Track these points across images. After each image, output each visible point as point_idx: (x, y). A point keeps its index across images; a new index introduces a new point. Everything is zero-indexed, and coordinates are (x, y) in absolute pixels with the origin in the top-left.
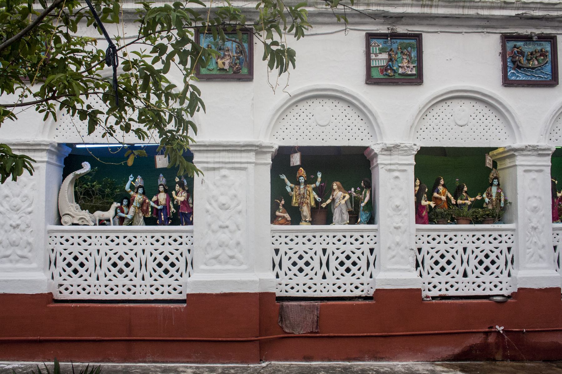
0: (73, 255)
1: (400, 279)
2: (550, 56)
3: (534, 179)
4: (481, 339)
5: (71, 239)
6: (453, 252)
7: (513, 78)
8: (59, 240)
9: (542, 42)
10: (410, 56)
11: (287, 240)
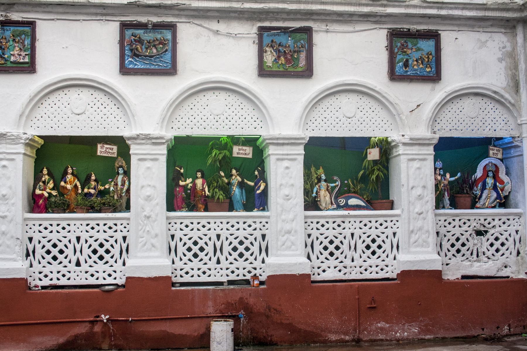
0: (98, 242)
3: (148, 168)
4: (86, 329)
6: (251, 239)
9: (162, 31)
10: (23, 43)
11: (319, 226)
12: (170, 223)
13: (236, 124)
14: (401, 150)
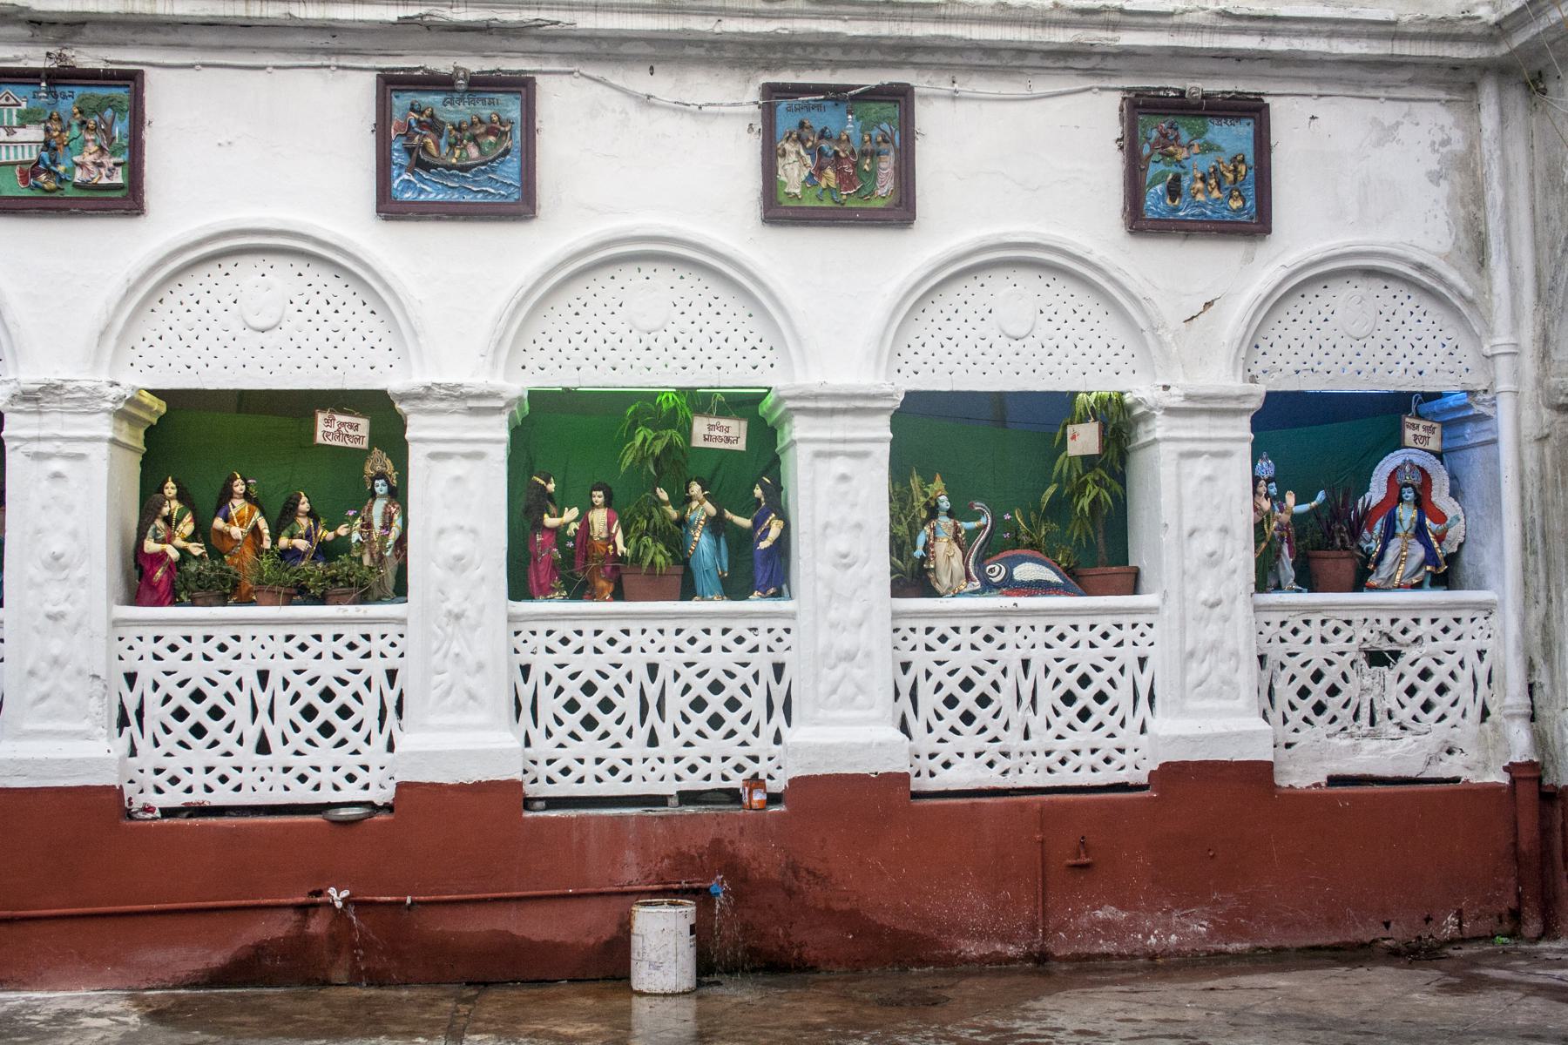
1: (53, 761)
2: (518, 133)
3: (458, 479)
4: (287, 926)
5: (701, 636)
6: (745, 675)
7: (408, 196)
8: (148, 647)
9: (496, 96)
10: (108, 132)
11: (932, 639)
12: (517, 634)
13: (560, 358)
14: (1160, 427)
